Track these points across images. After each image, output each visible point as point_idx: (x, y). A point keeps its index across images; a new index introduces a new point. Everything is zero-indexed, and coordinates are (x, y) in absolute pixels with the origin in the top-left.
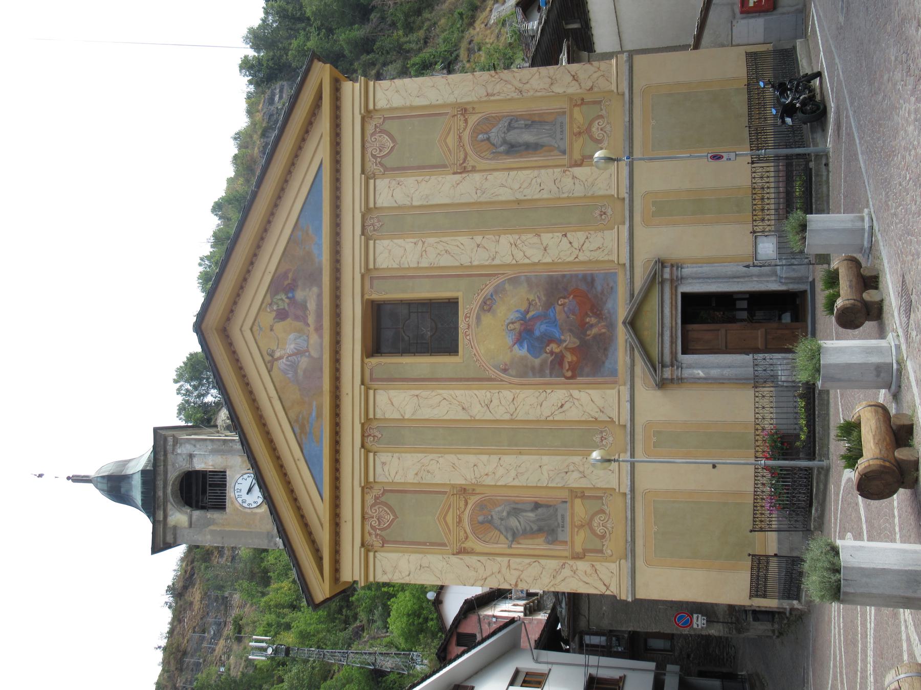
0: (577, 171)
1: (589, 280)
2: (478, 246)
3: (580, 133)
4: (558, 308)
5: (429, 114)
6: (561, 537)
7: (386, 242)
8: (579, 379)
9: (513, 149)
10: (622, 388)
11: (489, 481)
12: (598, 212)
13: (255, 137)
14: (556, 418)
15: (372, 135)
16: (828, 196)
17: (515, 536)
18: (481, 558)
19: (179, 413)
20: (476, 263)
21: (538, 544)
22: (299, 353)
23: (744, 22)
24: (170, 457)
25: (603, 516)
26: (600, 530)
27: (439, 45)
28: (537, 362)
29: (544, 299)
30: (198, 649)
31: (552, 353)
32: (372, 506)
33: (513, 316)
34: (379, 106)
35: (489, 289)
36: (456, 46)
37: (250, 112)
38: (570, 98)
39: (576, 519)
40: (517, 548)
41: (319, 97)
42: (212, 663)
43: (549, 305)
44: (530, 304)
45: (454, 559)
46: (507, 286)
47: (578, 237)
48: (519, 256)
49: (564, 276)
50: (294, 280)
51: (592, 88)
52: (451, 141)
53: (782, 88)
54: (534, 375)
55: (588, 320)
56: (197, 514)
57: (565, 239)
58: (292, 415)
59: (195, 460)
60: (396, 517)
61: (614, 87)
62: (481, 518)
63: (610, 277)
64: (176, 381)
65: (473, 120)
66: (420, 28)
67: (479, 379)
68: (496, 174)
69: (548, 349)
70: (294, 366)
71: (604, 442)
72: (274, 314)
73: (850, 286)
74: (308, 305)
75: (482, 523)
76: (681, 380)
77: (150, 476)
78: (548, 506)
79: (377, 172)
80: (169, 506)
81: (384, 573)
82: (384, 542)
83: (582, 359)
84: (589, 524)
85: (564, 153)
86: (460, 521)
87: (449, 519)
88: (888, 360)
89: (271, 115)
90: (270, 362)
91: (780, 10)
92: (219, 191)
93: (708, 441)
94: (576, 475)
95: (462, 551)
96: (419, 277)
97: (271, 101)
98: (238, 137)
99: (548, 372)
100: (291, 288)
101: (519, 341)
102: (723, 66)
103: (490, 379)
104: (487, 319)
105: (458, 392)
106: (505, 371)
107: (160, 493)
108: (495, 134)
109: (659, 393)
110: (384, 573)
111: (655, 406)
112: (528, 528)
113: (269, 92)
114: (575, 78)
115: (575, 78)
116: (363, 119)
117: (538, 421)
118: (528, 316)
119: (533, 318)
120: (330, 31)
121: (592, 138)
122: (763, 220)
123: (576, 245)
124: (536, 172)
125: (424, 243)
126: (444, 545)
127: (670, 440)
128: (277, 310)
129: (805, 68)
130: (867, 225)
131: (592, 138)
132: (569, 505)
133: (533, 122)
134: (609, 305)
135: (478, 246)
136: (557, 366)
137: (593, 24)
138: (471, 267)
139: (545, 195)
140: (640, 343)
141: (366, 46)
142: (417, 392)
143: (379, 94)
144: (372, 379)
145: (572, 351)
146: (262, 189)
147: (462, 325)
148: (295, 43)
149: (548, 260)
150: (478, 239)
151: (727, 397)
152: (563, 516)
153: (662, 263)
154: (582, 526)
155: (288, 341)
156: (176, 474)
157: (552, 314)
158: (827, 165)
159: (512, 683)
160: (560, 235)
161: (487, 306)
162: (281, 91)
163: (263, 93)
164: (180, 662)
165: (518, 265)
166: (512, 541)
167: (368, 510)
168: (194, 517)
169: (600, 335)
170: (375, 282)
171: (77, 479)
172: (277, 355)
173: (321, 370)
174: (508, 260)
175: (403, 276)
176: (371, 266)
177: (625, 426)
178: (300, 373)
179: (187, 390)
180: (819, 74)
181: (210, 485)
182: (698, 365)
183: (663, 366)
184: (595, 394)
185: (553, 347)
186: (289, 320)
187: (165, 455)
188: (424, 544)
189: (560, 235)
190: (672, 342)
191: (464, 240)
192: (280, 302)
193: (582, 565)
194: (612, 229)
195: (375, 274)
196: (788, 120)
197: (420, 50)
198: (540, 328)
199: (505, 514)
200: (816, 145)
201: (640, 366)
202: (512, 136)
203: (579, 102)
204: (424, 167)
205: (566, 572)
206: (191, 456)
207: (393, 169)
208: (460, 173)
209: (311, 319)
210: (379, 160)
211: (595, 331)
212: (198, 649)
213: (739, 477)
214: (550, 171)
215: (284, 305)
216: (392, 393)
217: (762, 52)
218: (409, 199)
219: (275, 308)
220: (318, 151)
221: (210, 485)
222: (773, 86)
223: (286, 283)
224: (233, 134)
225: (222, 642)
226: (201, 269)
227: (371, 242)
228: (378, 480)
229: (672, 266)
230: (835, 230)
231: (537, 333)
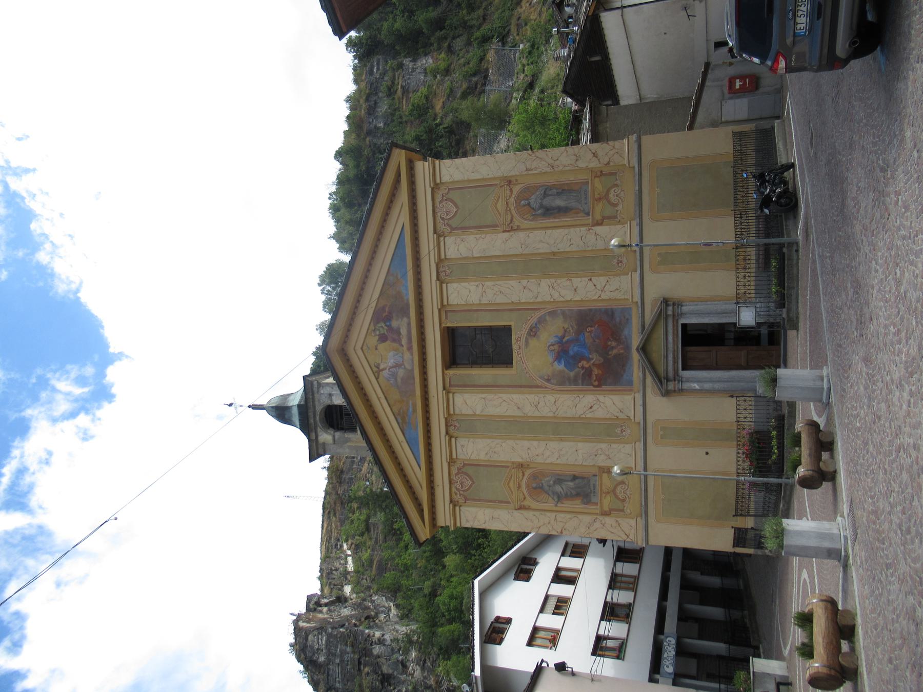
0: (598, 229)
1: (610, 313)
3: (600, 199)
4: (587, 334)
5: (483, 186)
6: (593, 500)
7: (455, 285)
8: (604, 387)
9: (548, 212)
10: (636, 395)
11: (539, 460)
12: (615, 261)
13: (362, 101)
14: (587, 416)
15: (441, 202)
16: (798, 276)
17: (560, 498)
18: (537, 513)
19: (324, 307)
20: (523, 301)
21: (577, 505)
22: (397, 366)
23: (731, 102)
24: (316, 395)
26: (621, 496)
27: (494, 22)
28: (572, 374)
30: (350, 469)
31: (583, 367)
32: (456, 475)
33: (553, 340)
34: (444, 180)
35: (534, 320)
36: (508, 23)
37: (356, 81)
38: (592, 171)
39: (604, 488)
41: (398, 174)
42: (360, 479)
43: (580, 331)
44: (565, 331)
45: (516, 513)
46: (547, 318)
47: (600, 281)
48: (556, 296)
49: (590, 310)
50: (390, 313)
51: (608, 163)
52: (500, 205)
53: (761, 178)
55: (609, 343)
57: (590, 283)
58: (395, 410)
59: (334, 398)
60: (473, 482)
61: (626, 162)
62: (534, 485)
63: (626, 311)
64: (320, 285)
65: (516, 189)
66: (479, 7)
67: (530, 387)
68: (536, 232)
70: (394, 375)
72: (377, 337)
73: (810, 455)
75: (535, 488)
76: (681, 391)
77: (304, 409)
78: (583, 478)
79: (446, 231)
80: (319, 429)
81: (467, 521)
82: (466, 499)
83: (607, 373)
84: (614, 491)
85: (588, 214)
86: (519, 487)
87: (511, 484)
88: (838, 546)
89: (372, 84)
90: (377, 373)
91: (761, 90)
92: (338, 141)
93: (704, 435)
94: (603, 457)
95: (521, 508)
96: (481, 310)
97: (371, 72)
98: (349, 99)
99: (580, 381)
100: (388, 319)
101: (558, 358)
102: (712, 144)
103: (537, 387)
104: (533, 342)
105: (514, 396)
106: (548, 380)
107: (312, 421)
108: (534, 200)
109: (664, 399)
110: (467, 521)
111: (662, 408)
113: (369, 65)
114: (595, 155)
115: (595, 155)
116: (433, 190)
117: (574, 418)
118: (564, 340)
119: (567, 341)
120: (412, 13)
121: (609, 202)
122: (745, 269)
123: (599, 287)
124: (566, 231)
126: (508, 503)
127: (674, 433)
129: (782, 160)
130: (825, 387)
131: (609, 202)
132: (598, 478)
133: (563, 190)
134: (626, 332)
137: (611, 56)
138: (520, 303)
139: (574, 248)
140: (650, 364)
141: (438, 24)
142: (483, 396)
143: (444, 171)
144: (451, 385)
145: (598, 366)
146: (361, 248)
147: (515, 347)
148: (385, 25)
149: (578, 298)
150: (524, 282)
151: (715, 403)
152: (594, 486)
153: (666, 302)
154: (608, 493)
155: (388, 356)
156: (321, 407)
158: (797, 251)
159: (563, 555)
160: (586, 279)
161: (533, 332)
162: (378, 64)
163: (365, 66)
164: (339, 477)
165: (554, 302)
167: (453, 477)
168: (337, 437)
170: (449, 314)
171: (254, 407)
172: (382, 367)
173: (414, 378)
174: (548, 299)
175: (469, 310)
176: (445, 303)
177: (639, 423)
178: (399, 380)
179: (328, 291)
180: (792, 166)
181: (346, 415)
182: (695, 378)
183: (668, 381)
184: (616, 398)
185: (584, 363)
186: (388, 343)
187: (313, 394)
188: (495, 502)
189: (586, 279)
190: (674, 362)
191: (513, 283)
193: (609, 520)
194: (627, 274)
195: (449, 308)
196: (767, 211)
197: (480, 25)
198: (573, 349)
200: (789, 236)
201: (649, 380)
202: (547, 202)
203: (599, 174)
204: (480, 227)
205: (597, 525)
206: (331, 395)
207: (456, 229)
208: (508, 231)
209: (404, 341)
211: (615, 351)
212: (350, 469)
213: (726, 461)
214: (578, 229)
215: (384, 330)
216: (466, 396)
217: (746, 132)
220: (400, 217)
221: (346, 415)
222: (754, 177)
224: (344, 97)
225: (366, 465)
226: (330, 201)
227: (444, 285)
228: (461, 456)
229: (674, 304)
230: (801, 388)
231: (571, 353)
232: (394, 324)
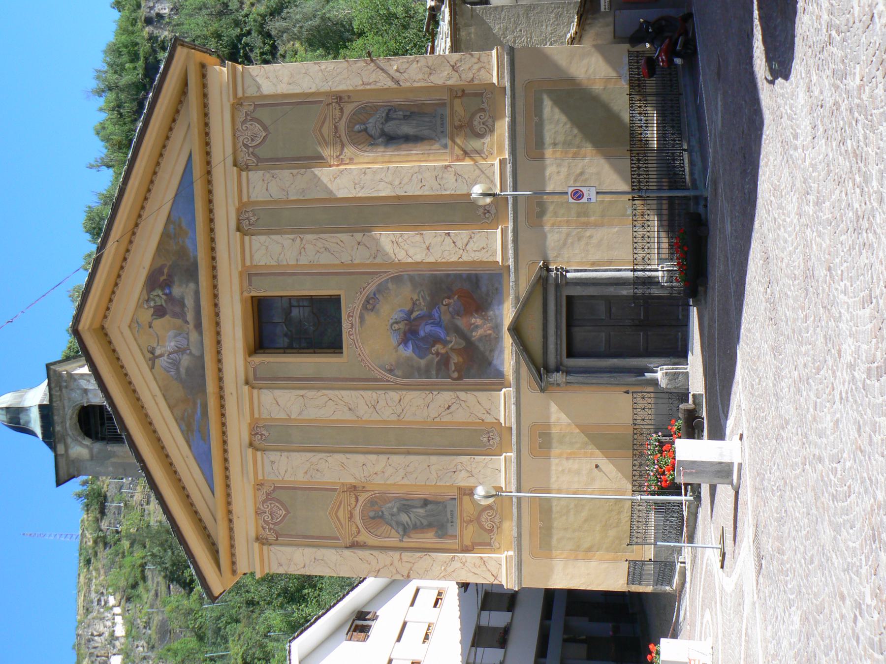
2: (359, 243)
4: (443, 308)
17: (406, 530)
25: (491, 512)
29: (428, 299)
31: (437, 354)
39: (465, 515)
40: (408, 542)
43: (434, 303)
46: (390, 285)
54: (420, 376)
56: (98, 446)
62: (372, 514)
65: (363, 497)
69: (434, 350)
70: (176, 364)
71: (491, 442)
72: (152, 310)
74: (186, 302)
80: (69, 440)
84: (478, 519)
86: (351, 516)
100: (168, 284)
101: (405, 341)
104: (370, 318)
106: (390, 371)
112: (418, 523)
125: (302, 240)
128: (154, 307)
135: (359, 243)
136: (443, 367)
144: (256, 378)
154: (471, 521)
157: (436, 315)
161: (370, 304)
166: (403, 536)
169: (486, 336)
172: (158, 352)
185: (439, 347)
186: (167, 317)
192: (157, 299)
198: (425, 330)
199: (395, 510)
204: (299, 159)
209: (190, 316)
210: (251, 150)
211: (480, 332)
216: (278, 393)
218: (285, 193)
219: (152, 304)
223: (162, 279)
232: (177, 291)
